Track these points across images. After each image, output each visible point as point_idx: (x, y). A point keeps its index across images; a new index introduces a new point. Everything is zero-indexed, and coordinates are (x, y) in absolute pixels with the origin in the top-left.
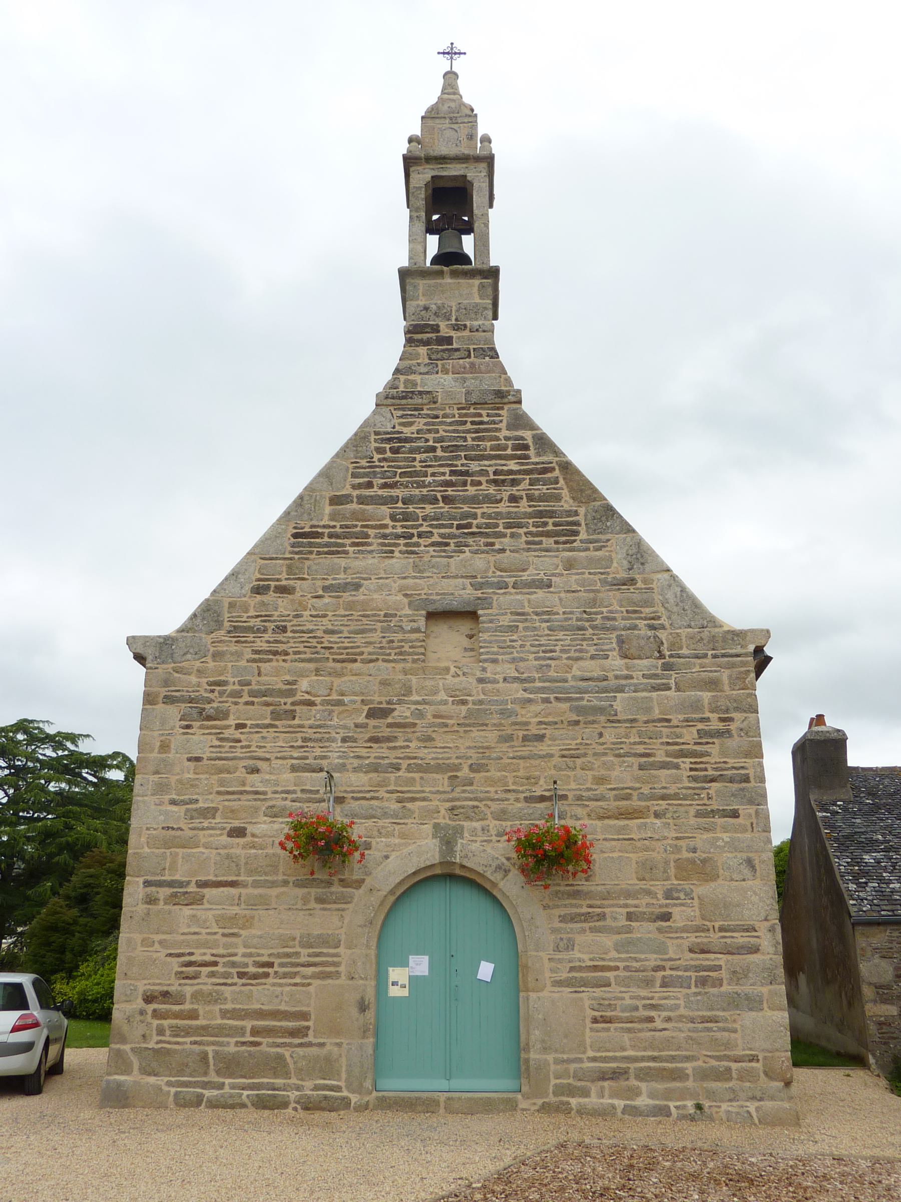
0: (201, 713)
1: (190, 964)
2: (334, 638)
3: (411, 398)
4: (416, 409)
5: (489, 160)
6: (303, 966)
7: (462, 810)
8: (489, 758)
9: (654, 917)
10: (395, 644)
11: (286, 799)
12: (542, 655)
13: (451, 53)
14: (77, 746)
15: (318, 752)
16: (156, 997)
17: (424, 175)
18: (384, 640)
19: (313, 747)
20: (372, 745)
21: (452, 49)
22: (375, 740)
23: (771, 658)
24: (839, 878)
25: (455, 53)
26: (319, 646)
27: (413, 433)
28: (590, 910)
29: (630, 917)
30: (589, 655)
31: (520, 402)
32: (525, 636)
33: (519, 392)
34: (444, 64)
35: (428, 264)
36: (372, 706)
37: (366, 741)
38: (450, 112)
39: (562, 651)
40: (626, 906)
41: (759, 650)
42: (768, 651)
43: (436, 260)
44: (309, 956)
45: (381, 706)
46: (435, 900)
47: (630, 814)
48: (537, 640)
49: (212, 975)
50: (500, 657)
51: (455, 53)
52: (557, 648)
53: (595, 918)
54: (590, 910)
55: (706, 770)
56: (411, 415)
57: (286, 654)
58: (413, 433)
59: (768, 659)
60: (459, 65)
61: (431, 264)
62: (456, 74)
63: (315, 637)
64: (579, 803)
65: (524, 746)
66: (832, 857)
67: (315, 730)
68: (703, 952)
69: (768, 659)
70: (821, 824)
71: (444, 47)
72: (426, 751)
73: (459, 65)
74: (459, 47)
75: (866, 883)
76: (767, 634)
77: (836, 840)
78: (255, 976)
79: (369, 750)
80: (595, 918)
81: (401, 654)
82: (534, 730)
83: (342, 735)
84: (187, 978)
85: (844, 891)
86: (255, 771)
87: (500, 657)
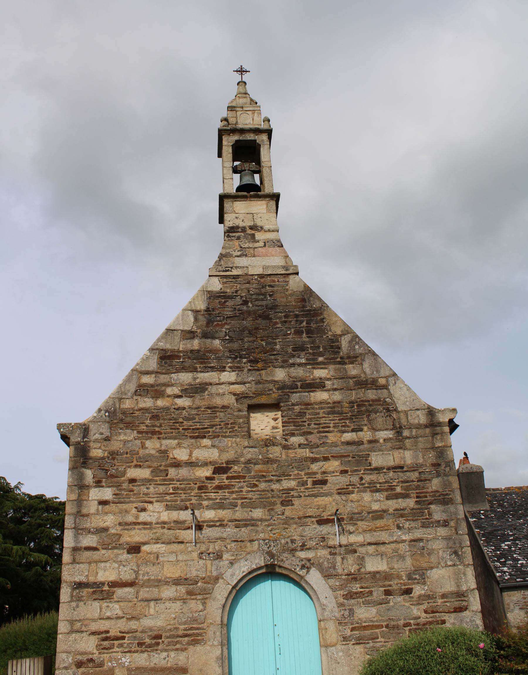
0: (107, 475)
1: (106, 639)
2: (190, 423)
3: (231, 271)
4: (234, 278)
5: (269, 132)
6: (181, 637)
7: (278, 531)
8: (293, 496)
9: (402, 592)
10: (229, 426)
11: (164, 527)
12: (321, 430)
13: (241, 71)
14: (129, 391)
15: (183, 496)
16: (84, 663)
17: (229, 141)
18: (222, 424)
19: (181, 494)
20: (218, 491)
21: (241, 69)
22: (219, 487)
23: (458, 426)
24: (488, 559)
25: (244, 71)
26: (181, 428)
27: (233, 293)
28: (362, 590)
29: (388, 593)
30: (350, 429)
31: (297, 274)
32: (311, 419)
33: (296, 266)
34: (238, 77)
35: (235, 192)
36: (217, 466)
37: (213, 489)
38: (243, 100)
39: (334, 427)
40: (384, 586)
41: (451, 421)
42: (456, 421)
43: (239, 189)
44: (184, 630)
45: (222, 465)
46: (266, 589)
47: (382, 527)
48: (318, 421)
49: (121, 645)
50: (296, 432)
51: (244, 71)
52: (331, 425)
53: (366, 595)
54: (362, 590)
55: (426, 497)
56: (231, 282)
57: (160, 433)
58: (233, 293)
59: (457, 426)
60: (246, 77)
61: (236, 191)
62: (245, 83)
63: (178, 423)
64: (351, 522)
65: (314, 488)
66: (482, 546)
67: (181, 483)
68: (433, 612)
69: (457, 426)
70: (473, 526)
71: (237, 67)
72: (252, 493)
73: (246, 77)
74: (245, 67)
75: (505, 562)
76: (454, 410)
77: (483, 535)
78: (150, 646)
79: (216, 494)
80: (366, 595)
81: (233, 431)
82: (319, 477)
83: (198, 485)
84: (104, 648)
85: (493, 567)
86: (144, 510)
87: (296, 432)
